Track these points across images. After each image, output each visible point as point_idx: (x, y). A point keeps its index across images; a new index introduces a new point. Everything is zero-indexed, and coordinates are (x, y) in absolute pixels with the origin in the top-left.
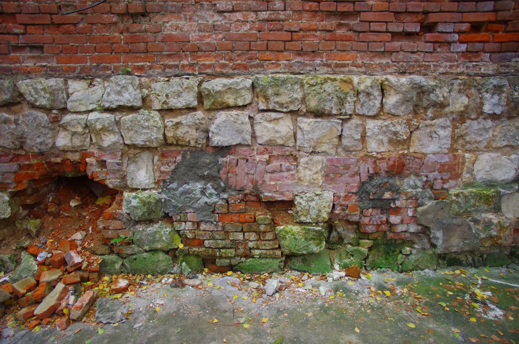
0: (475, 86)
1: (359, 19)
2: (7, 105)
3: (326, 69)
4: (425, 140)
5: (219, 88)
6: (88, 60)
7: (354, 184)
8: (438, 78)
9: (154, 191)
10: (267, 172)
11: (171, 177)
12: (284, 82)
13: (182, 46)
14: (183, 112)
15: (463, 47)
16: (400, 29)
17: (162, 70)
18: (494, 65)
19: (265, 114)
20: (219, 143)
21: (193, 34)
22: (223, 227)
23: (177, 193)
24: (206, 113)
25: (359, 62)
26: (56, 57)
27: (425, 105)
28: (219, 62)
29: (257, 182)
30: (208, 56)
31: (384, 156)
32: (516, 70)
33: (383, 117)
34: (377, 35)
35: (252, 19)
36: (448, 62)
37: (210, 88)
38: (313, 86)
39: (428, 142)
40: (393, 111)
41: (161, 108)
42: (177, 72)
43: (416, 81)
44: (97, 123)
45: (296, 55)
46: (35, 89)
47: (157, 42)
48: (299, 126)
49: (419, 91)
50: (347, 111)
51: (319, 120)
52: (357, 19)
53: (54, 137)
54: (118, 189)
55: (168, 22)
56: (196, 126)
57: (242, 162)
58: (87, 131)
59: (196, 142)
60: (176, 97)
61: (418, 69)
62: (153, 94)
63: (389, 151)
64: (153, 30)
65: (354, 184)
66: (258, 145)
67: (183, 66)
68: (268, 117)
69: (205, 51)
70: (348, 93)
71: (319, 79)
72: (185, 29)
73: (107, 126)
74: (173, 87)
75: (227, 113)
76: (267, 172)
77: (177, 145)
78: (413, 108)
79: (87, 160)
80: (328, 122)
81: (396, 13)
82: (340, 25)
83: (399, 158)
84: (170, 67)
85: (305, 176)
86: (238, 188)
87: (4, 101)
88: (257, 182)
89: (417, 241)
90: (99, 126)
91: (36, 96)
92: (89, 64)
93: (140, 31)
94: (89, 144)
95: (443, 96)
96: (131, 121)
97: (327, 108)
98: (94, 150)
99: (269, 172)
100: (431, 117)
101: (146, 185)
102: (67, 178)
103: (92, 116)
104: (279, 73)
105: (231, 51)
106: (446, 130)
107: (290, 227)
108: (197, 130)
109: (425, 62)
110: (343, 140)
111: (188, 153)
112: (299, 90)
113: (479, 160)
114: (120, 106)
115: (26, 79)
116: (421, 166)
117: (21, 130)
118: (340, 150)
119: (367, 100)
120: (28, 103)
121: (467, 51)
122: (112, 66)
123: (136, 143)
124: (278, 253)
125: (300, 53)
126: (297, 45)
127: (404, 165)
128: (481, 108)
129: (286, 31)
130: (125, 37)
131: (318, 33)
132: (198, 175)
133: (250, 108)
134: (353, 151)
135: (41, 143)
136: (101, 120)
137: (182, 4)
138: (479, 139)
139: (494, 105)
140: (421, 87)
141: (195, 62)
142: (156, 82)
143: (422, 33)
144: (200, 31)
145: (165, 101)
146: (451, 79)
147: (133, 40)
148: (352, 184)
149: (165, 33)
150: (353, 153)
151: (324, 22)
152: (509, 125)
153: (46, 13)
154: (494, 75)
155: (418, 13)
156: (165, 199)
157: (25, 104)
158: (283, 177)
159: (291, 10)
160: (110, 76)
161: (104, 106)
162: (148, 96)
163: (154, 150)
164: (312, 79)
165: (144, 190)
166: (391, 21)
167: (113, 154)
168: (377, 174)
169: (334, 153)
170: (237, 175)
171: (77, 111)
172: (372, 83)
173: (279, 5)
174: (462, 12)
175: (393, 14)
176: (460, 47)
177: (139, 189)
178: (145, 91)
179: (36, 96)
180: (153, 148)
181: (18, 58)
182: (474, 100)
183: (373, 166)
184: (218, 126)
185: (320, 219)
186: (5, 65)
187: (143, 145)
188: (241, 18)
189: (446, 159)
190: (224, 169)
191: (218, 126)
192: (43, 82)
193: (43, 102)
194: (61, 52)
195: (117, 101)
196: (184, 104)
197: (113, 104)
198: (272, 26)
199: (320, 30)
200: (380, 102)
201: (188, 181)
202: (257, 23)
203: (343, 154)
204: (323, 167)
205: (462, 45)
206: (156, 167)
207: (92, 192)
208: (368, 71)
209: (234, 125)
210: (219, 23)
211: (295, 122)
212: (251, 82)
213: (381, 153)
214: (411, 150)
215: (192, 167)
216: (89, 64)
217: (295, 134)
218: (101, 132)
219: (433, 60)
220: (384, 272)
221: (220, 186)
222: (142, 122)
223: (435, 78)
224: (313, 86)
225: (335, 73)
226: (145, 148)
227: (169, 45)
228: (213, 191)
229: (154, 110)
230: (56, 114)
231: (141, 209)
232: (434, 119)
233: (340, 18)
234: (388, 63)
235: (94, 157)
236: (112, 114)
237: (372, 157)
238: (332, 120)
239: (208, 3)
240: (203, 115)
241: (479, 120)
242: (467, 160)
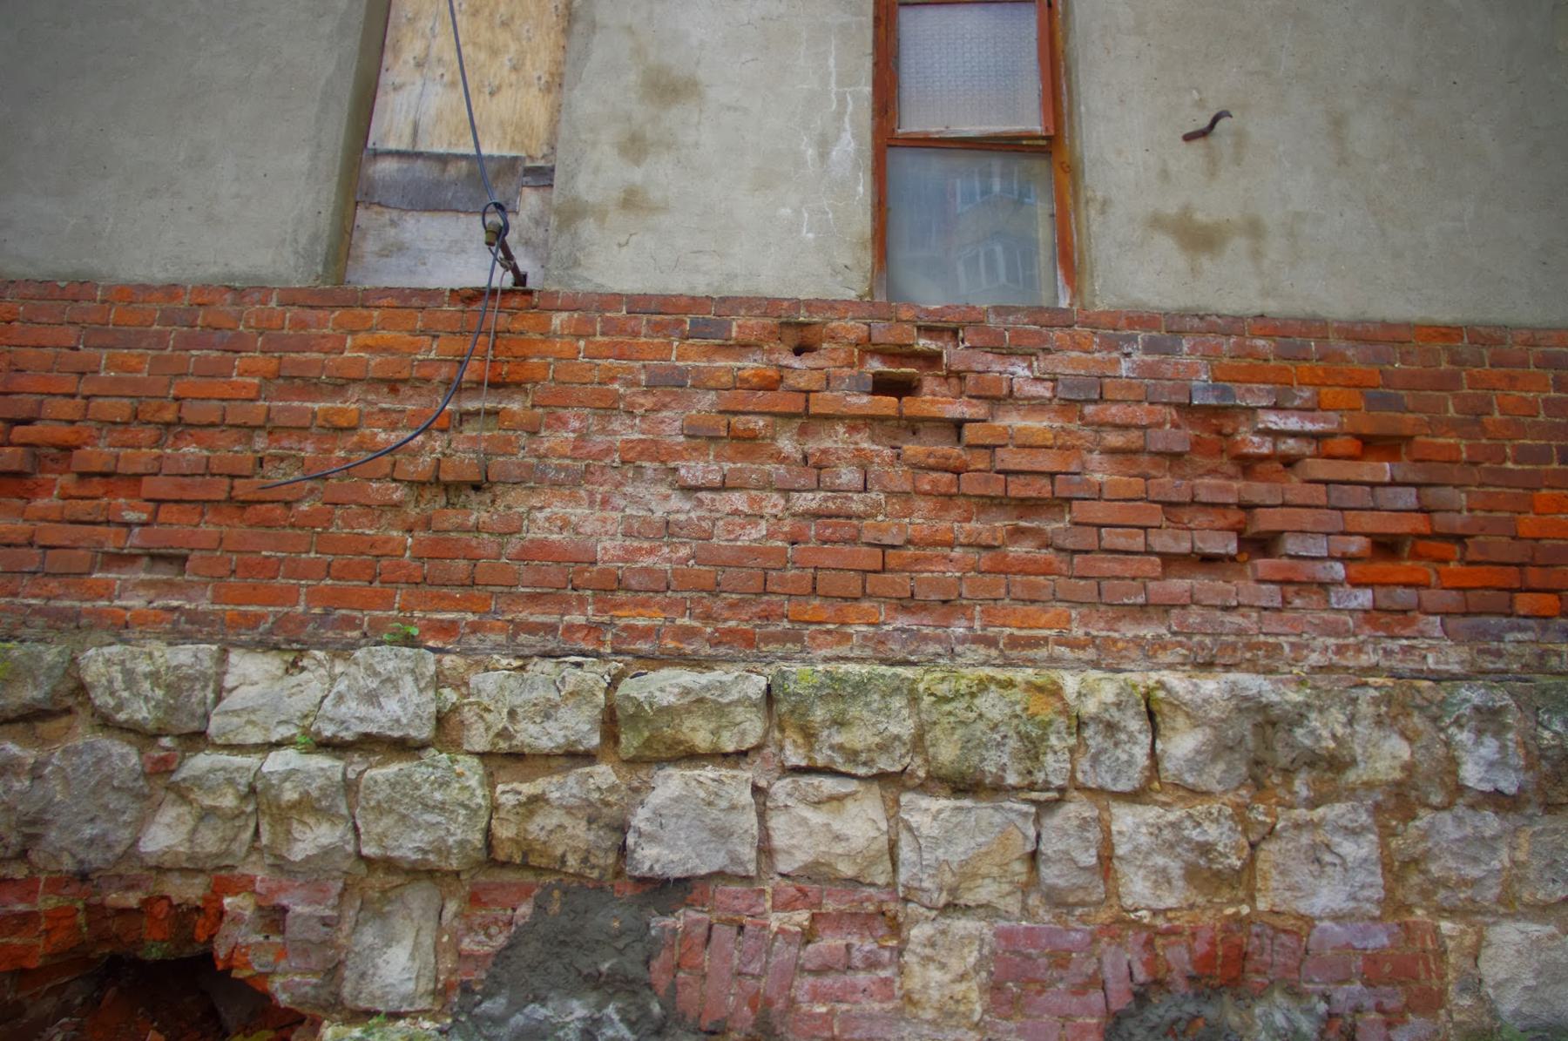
0: (1420, 708)
1: (1068, 517)
2: (30, 718)
3: (982, 651)
4: (1302, 873)
6: (303, 598)
7: (1089, 1021)
8: (1310, 683)
9: (427, 1024)
10: (803, 969)
11: (492, 976)
12: (861, 687)
13: (574, 573)
14: (554, 763)
15: (1364, 598)
16: (1185, 547)
17: (507, 637)
18: (1460, 649)
19: (804, 781)
20: (657, 867)
21: (608, 544)
24: (624, 771)
25: (1078, 632)
26: (215, 587)
27: (1283, 761)
28: (673, 621)
29: (769, 1002)
30: (645, 604)
31: (1177, 923)
32: (1523, 666)
33: (1161, 798)
34: (1124, 563)
35: (774, 511)
36: (1329, 635)
37: (641, 698)
38: (945, 700)
39: (1310, 879)
40: (1190, 779)
41: (488, 748)
42: (551, 645)
43: (1246, 689)
44: (288, 785)
45: (896, 610)
46: (130, 677)
47: (504, 560)
48: (906, 823)
49: (1259, 718)
50: (1051, 778)
51: (967, 803)
52: (1064, 517)
53: (141, 823)
54: (306, 1010)
55: (541, 508)
56: (589, 811)
57: (724, 933)
58: (250, 809)
59: (585, 860)
60: (538, 720)
61: (1248, 655)
62: (470, 704)
63: (1192, 907)
65: (1089, 1021)
66: (778, 878)
67: (570, 628)
68: (810, 789)
69: (637, 591)
70: (1050, 723)
71: (964, 681)
72: (587, 528)
73: (315, 794)
74: (532, 688)
75: (688, 773)
76: (803, 969)
77: (525, 866)
78: (1250, 769)
79: (227, 901)
80: (996, 809)
81: (1168, 505)
82: (1017, 534)
83: (1226, 930)
84: (532, 629)
85: (926, 987)
86: (706, 1023)
87: (24, 705)
88: (769, 1002)
90: (290, 794)
91: (126, 694)
92: (300, 609)
94: (244, 849)
95: (1334, 736)
96: (393, 785)
97: (990, 767)
98: (259, 871)
99: (810, 972)
100: (1306, 799)
101: (404, 998)
102: (140, 964)
103: (276, 762)
104: (847, 659)
105: (709, 592)
106: (1361, 840)
108: (590, 821)
109: (1266, 634)
110: (1042, 868)
111: (556, 894)
112: (905, 712)
113: (1490, 944)
114: (367, 736)
115: (110, 644)
116: (1302, 961)
117: (43, 797)
118: (1034, 900)
119: (1109, 744)
120: (95, 711)
121: (1376, 608)
122: (366, 617)
123: (396, 854)
125: (908, 604)
126: (899, 582)
127: (1245, 956)
128: (1455, 773)
129: (869, 544)
130: (419, 542)
131: (957, 552)
132: (580, 973)
133: (758, 761)
134: (1076, 905)
135: (92, 842)
136: (301, 776)
137: (587, 466)
138: (1473, 872)
139: (1491, 765)
140: (1264, 708)
141: (606, 619)
142: (487, 670)
143: (1245, 556)
145: (505, 729)
146: (1346, 684)
147: (439, 550)
148: (1080, 1020)
149: (530, 536)
150: (1079, 911)
151: (974, 525)
152: (1556, 831)
153: (220, 475)
154: (1466, 677)
155: (1226, 505)
157: (83, 714)
158: (854, 988)
159: (884, 492)
160: (354, 646)
161: (318, 733)
162: (456, 709)
163: (448, 880)
164: (943, 679)
165: (395, 1016)
166: (1157, 524)
167: (317, 890)
168: (1159, 983)
170: (704, 976)
171: (234, 742)
172: (1118, 695)
173: (850, 476)
174: (1342, 509)
175: (1159, 506)
176: (1356, 597)
177: (377, 1013)
178: (450, 695)
179: (126, 694)
180: (447, 874)
181: (109, 585)
182: (1427, 748)
183: (1145, 956)
184: (657, 814)
186: (67, 603)
187: (416, 861)
188: (746, 509)
189: (1380, 939)
191: (657, 814)
192: (157, 654)
193: (141, 712)
194: (234, 572)
195: (361, 720)
196: (562, 741)
197: (347, 729)
198: (829, 531)
199: (962, 545)
200: (1147, 750)
201: (543, 993)
202: (788, 521)
203: (1045, 916)
204: (982, 957)
205: (1359, 592)
206: (445, 939)
207: (212, 1014)
208: (1106, 658)
209: (706, 814)
210: (682, 517)
211: (893, 809)
212: (762, 682)
213: (1165, 911)
214: (1262, 905)
215: (563, 943)
216: (300, 609)
217: (893, 847)
218: (293, 813)
219: (1286, 629)
221: (646, 1013)
222: (426, 788)
223: (1301, 682)
224: (945, 700)
226: (420, 872)
227: (538, 570)
229: (469, 753)
230: (168, 749)
232: (1317, 806)
233: (1015, 513)
234: (1160, 637)
235: (254, 892)
236: (339, 758)
237: (1137, 924)
238: (1007, 805)
239: (657, 465)
240: (613, 778)
241: (1460, 810)
242: (1450, 944)
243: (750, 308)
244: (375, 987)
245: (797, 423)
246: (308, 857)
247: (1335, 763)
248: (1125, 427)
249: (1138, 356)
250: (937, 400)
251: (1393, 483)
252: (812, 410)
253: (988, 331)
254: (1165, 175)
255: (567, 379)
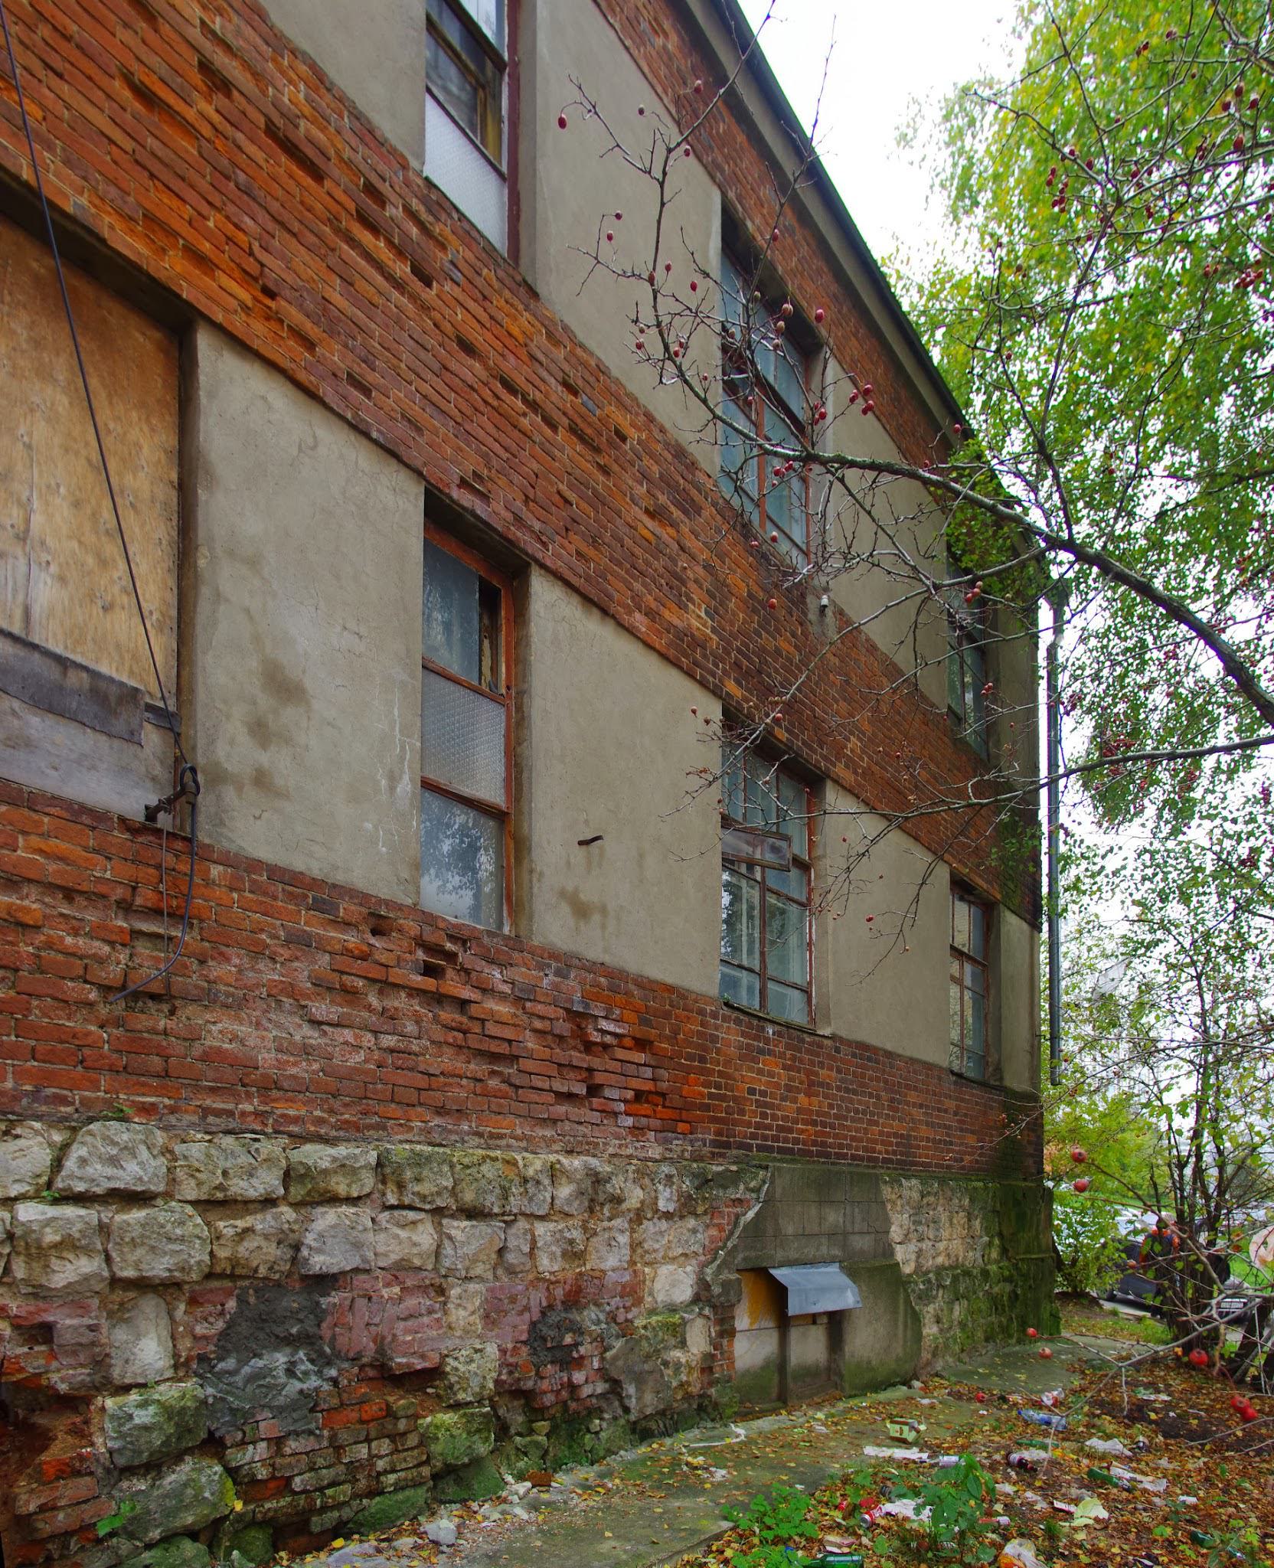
3: (477, 1140)
4: (604, 1249)
5: (325, 1164)
12: (429, 1159)
16: (565, 1089)
19: (396, 1213)
21: (266, 1055)
22: (333, 1438)
23: (239, 1379)
25: (519, 1132)
38: (468, 1167)
40: (566, 1209)
42: (232, 1125)
44: (48, 1230)
55: (214, 1023)
57: (361, 1302)
59: (271, 1269)
64: (183, 1034)
67: (243, 1114)
72: (251, 1042)
73: (77, 1235)
77: (232, 1277)
82: (493, 1073)
86: (351, 1355)
88: (383, 1338)
89: (604, 1405)
90: (51, 1237)
93: (154, 1031)
101: (157, 1372)
107: (440, 1416)
118: (500, 1272)
123: (149, 1274)
124: (426, 1471)
125: (441, 1111)
132: (277, 1337)
138: (657, 1246)
140: (597, 1174)
141: (267, 1108)
144: (279, 1050)
149: (208, 1043)
156: (215, 1397)
158: (422, 1326)
168: (550, 1307)
169: (491, 1277)
185: (486, 1393)
188: (351, 1040)
189: (627, 1278)
190: (329, 1318)
195: (109, 1179)
210: (313, 1042)
218: (53, 1252)
220: (572, 1469)
222: (169, 1226)
224: (468, 1167)
225: (489, 1148)
227: (217, 1069)
228: (310, 1366)
231: (161, 1429)
237: (544, 1280)
243: (351, 898)
244: (135, 1368)
245: (378, 986)
246: (70, 1284)
247: (617, 1200)
248: (542, 1018)
249: (551, 977)
250: (453, 985)
251: (645, 1065)
252: (391, 980)
253: (484, 946)
254: (568, 863)
255: (226, 922)
